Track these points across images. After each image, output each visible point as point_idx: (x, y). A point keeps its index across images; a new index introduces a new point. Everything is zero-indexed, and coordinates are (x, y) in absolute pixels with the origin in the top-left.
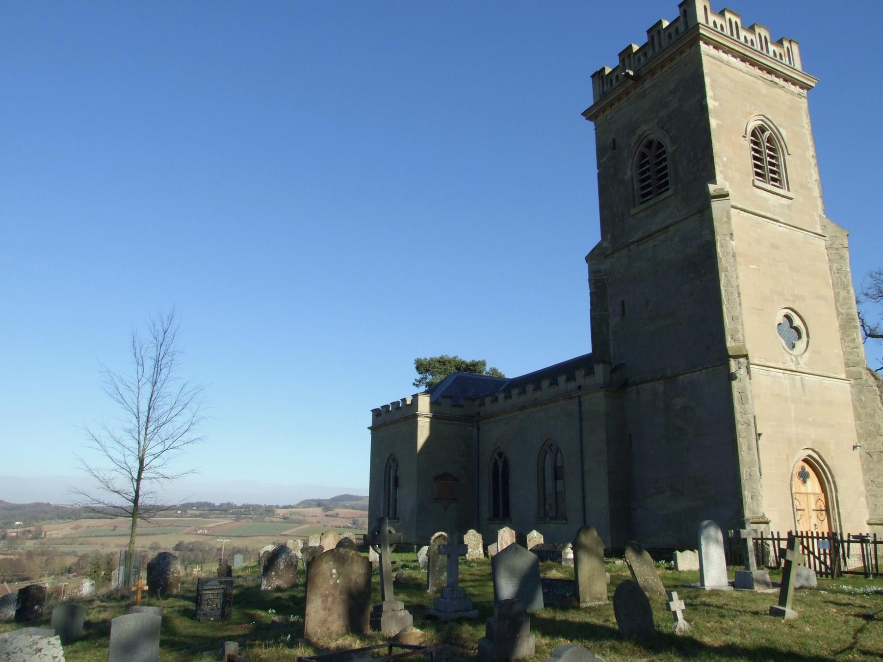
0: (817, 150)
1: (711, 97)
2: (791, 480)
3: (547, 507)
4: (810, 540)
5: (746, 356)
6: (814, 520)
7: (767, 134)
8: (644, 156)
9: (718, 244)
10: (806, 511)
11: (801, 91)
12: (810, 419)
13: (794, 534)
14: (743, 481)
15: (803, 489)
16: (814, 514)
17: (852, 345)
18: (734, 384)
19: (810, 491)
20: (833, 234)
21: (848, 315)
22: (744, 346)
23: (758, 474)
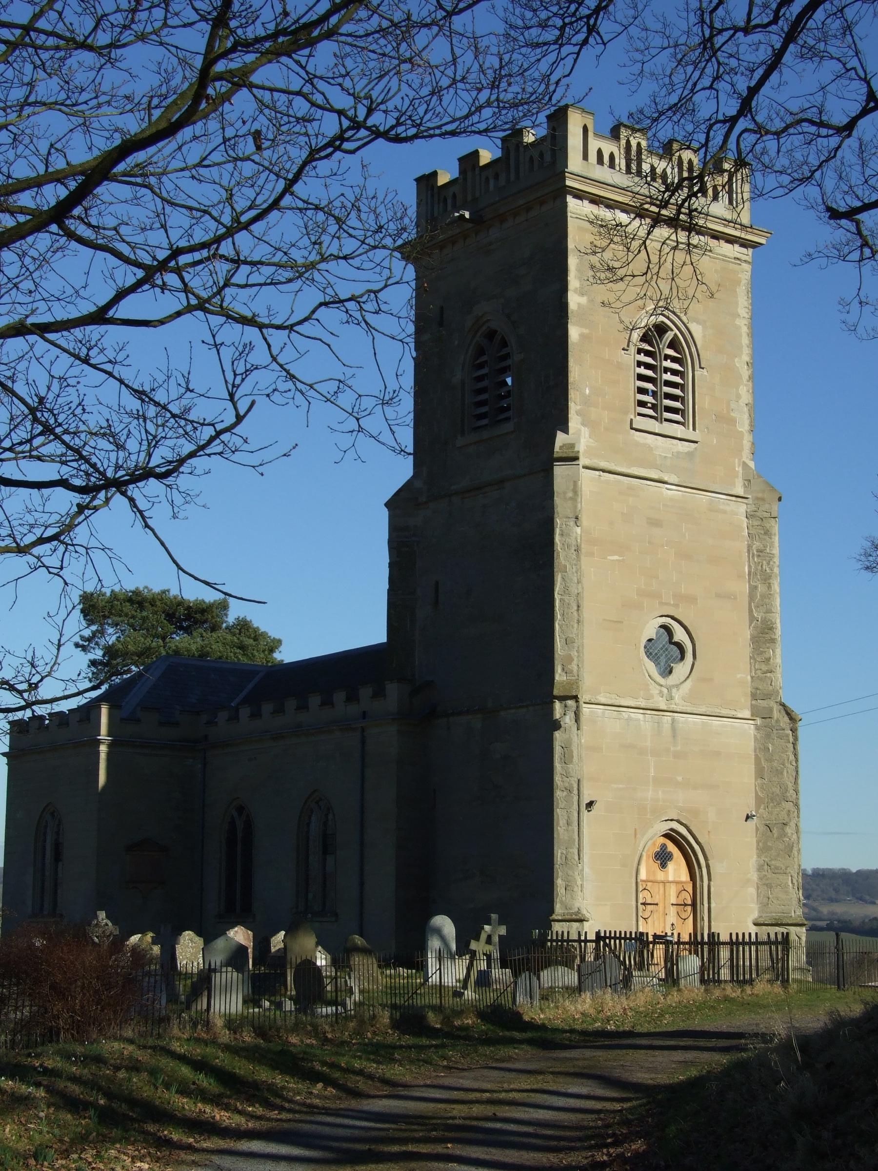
0: (753, 356)
1: (575, 291)
2: (639, 864)
3: (310, 896)
4: (618, 941)
5: (576, 698)
6: (672, 917)
7: (669, 336)
8: (481, 352)
9: (557, 531)
10: (661, 905)
11: (744, 250)
12: (680, 779)
13: (603, 935)
14: (556, 866)
15: (660, 875)
16: (673, 911)
17: (764, 668)
18: (557, 734)
19: (671, 879)
20: (760, 495)
21: (764, 621)
22: (577, 682)
23: (576, 857)
